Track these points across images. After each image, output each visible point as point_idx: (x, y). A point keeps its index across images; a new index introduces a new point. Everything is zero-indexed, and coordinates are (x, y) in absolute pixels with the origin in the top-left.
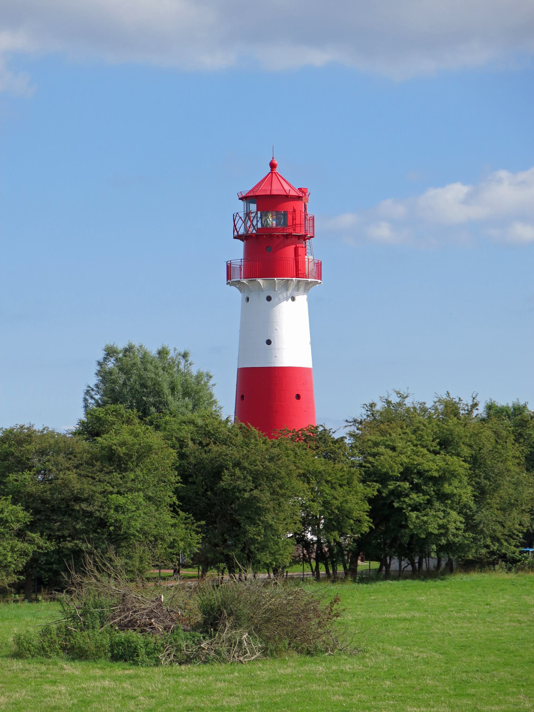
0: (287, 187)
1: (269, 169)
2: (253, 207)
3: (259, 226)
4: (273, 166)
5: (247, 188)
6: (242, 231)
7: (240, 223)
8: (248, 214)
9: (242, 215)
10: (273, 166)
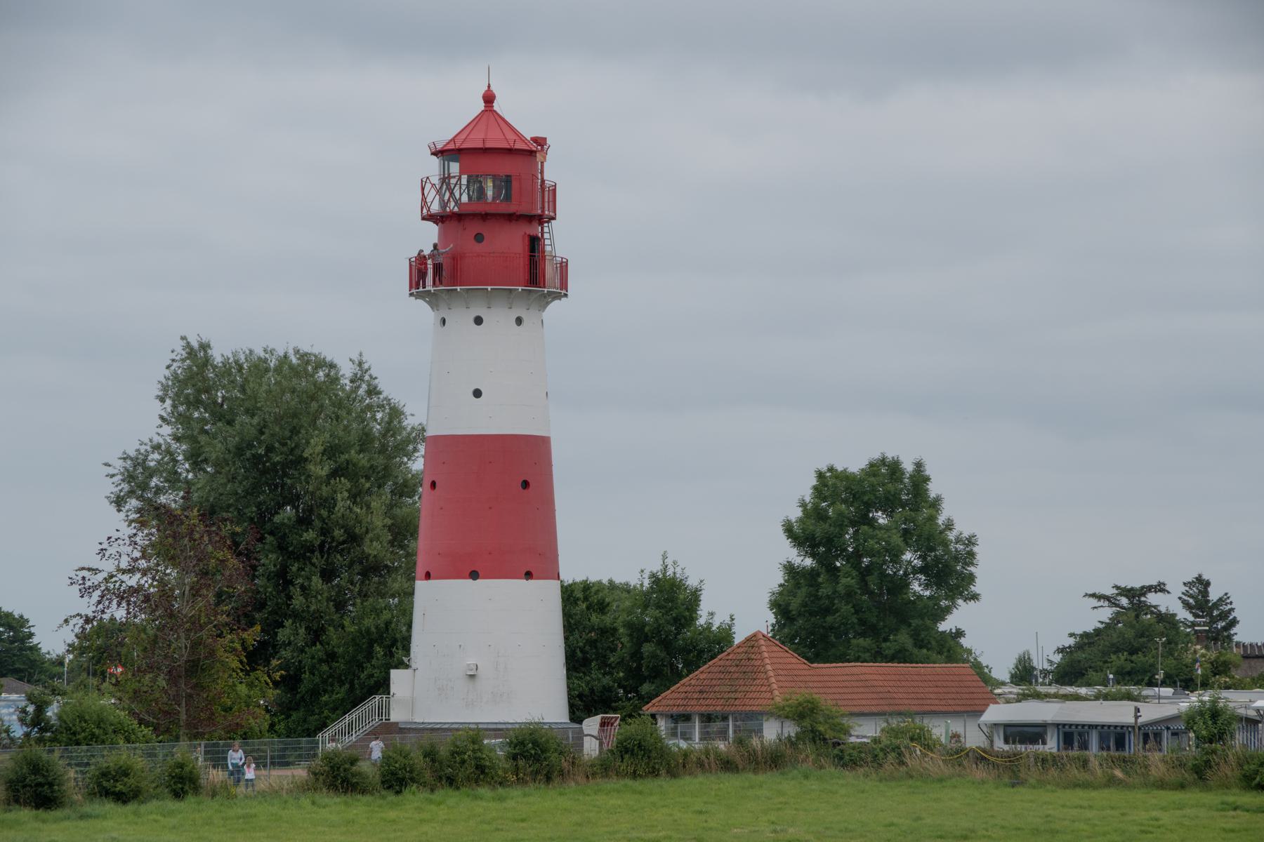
0: (511, 136)
1: (481, 106)
2: (455, 168)
3: (465, 199)
4: (489, 99)
6: (435, 208)
7: (431, 194)
8: (445, 179)
9: (435, 180)
10: (489, 99)
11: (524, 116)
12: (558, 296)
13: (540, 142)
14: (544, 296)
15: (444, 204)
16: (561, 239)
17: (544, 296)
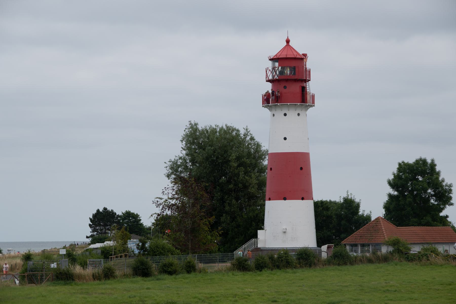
2: (277, 64)
4: (288, 41)
5: (273, 54)
6: (271, 78)
7: (269, 73)
8: (274, 68)
9: (271, 69)
10: (288, 41)
11: (299, 47)
12: (311, 106)
13: (305, 55)
14: (307, 106)
15: (273, 76)
16: (312, 87)
17: (307, 106)
